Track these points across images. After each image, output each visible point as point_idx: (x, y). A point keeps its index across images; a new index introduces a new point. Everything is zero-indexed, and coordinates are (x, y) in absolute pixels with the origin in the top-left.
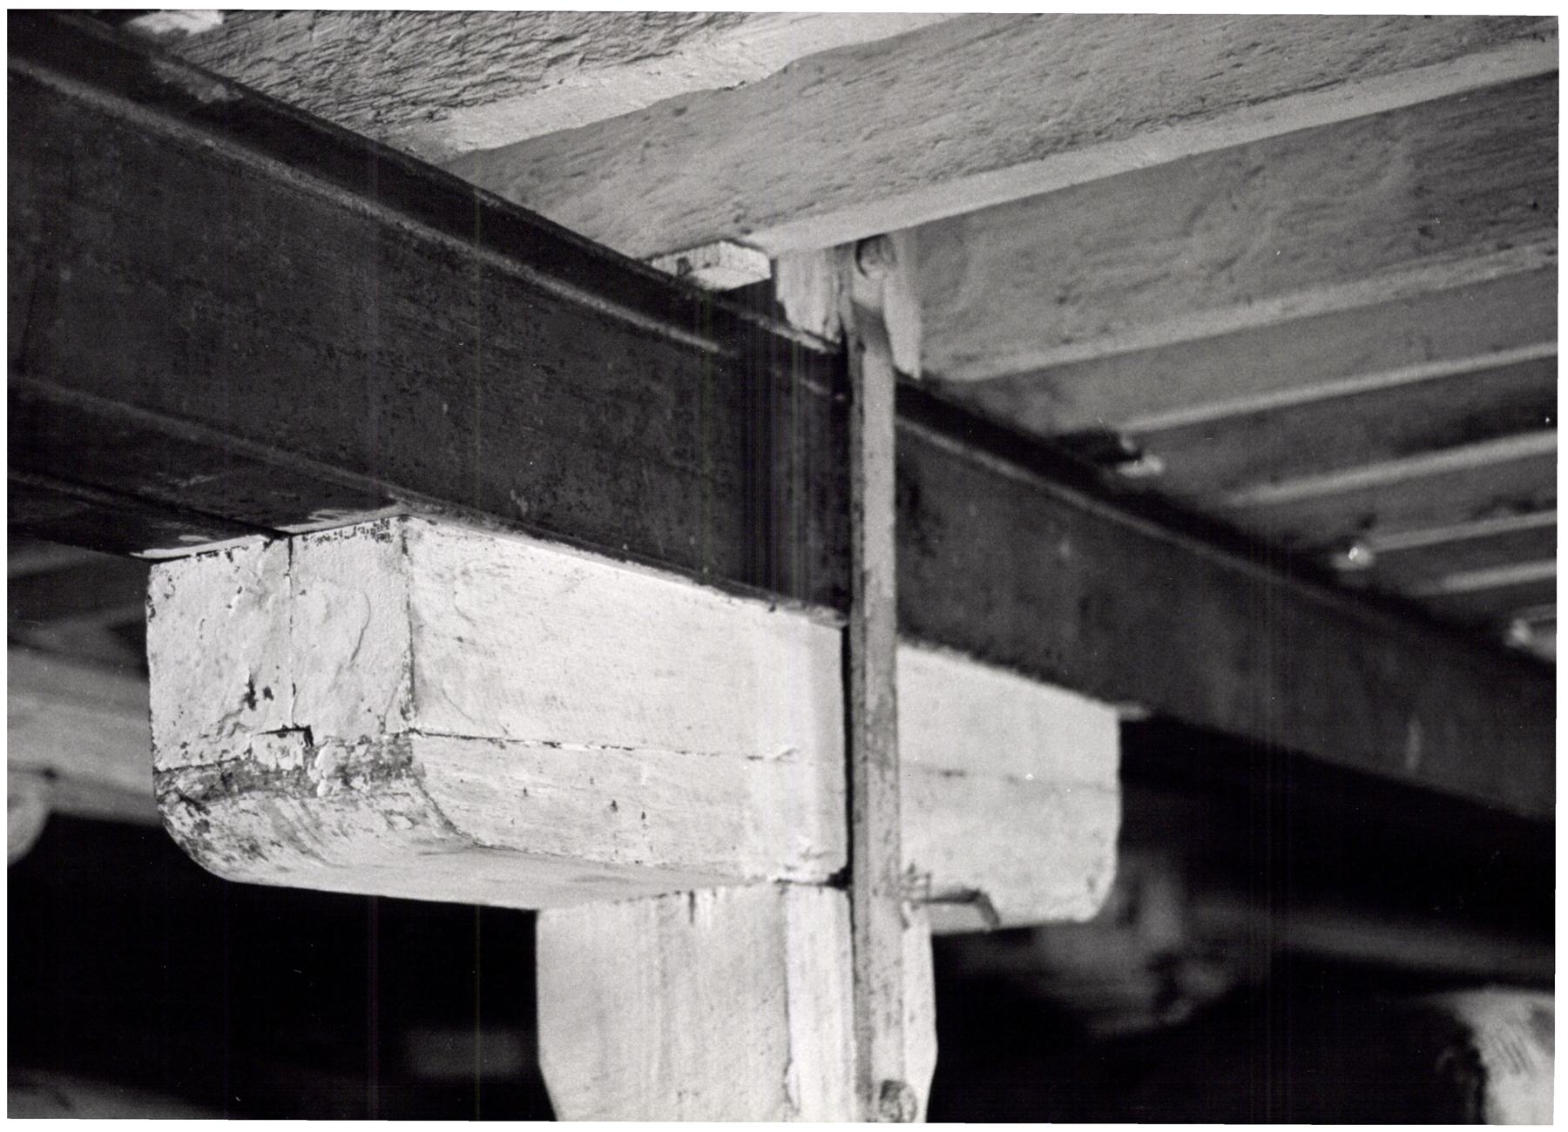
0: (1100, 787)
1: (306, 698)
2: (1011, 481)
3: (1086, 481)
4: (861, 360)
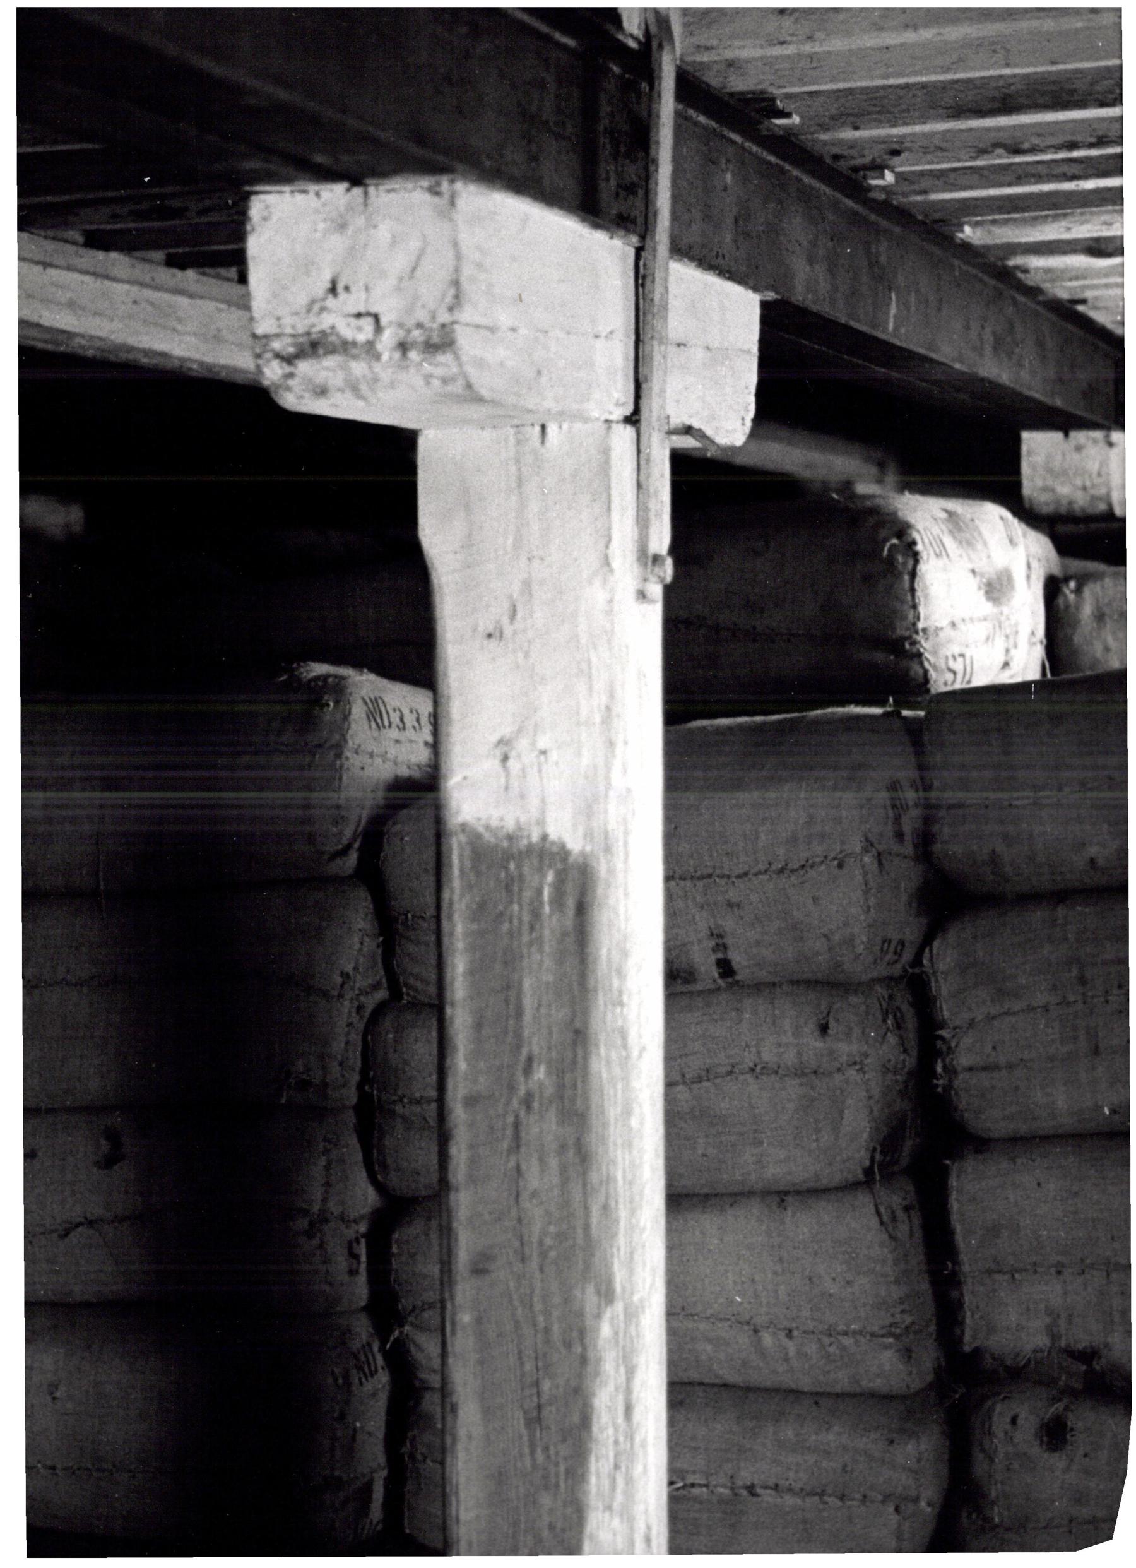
0: (749, 352)
1: (377, 292)
2: (705, 128)
3: (750, 130)
4: (661, 56)
